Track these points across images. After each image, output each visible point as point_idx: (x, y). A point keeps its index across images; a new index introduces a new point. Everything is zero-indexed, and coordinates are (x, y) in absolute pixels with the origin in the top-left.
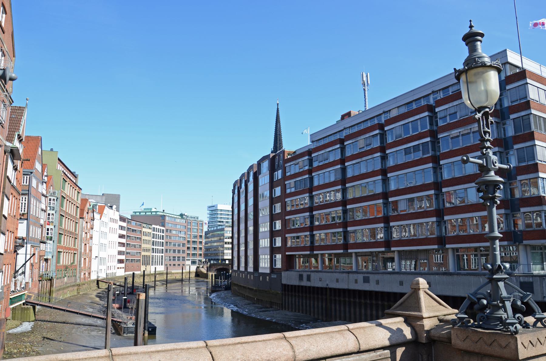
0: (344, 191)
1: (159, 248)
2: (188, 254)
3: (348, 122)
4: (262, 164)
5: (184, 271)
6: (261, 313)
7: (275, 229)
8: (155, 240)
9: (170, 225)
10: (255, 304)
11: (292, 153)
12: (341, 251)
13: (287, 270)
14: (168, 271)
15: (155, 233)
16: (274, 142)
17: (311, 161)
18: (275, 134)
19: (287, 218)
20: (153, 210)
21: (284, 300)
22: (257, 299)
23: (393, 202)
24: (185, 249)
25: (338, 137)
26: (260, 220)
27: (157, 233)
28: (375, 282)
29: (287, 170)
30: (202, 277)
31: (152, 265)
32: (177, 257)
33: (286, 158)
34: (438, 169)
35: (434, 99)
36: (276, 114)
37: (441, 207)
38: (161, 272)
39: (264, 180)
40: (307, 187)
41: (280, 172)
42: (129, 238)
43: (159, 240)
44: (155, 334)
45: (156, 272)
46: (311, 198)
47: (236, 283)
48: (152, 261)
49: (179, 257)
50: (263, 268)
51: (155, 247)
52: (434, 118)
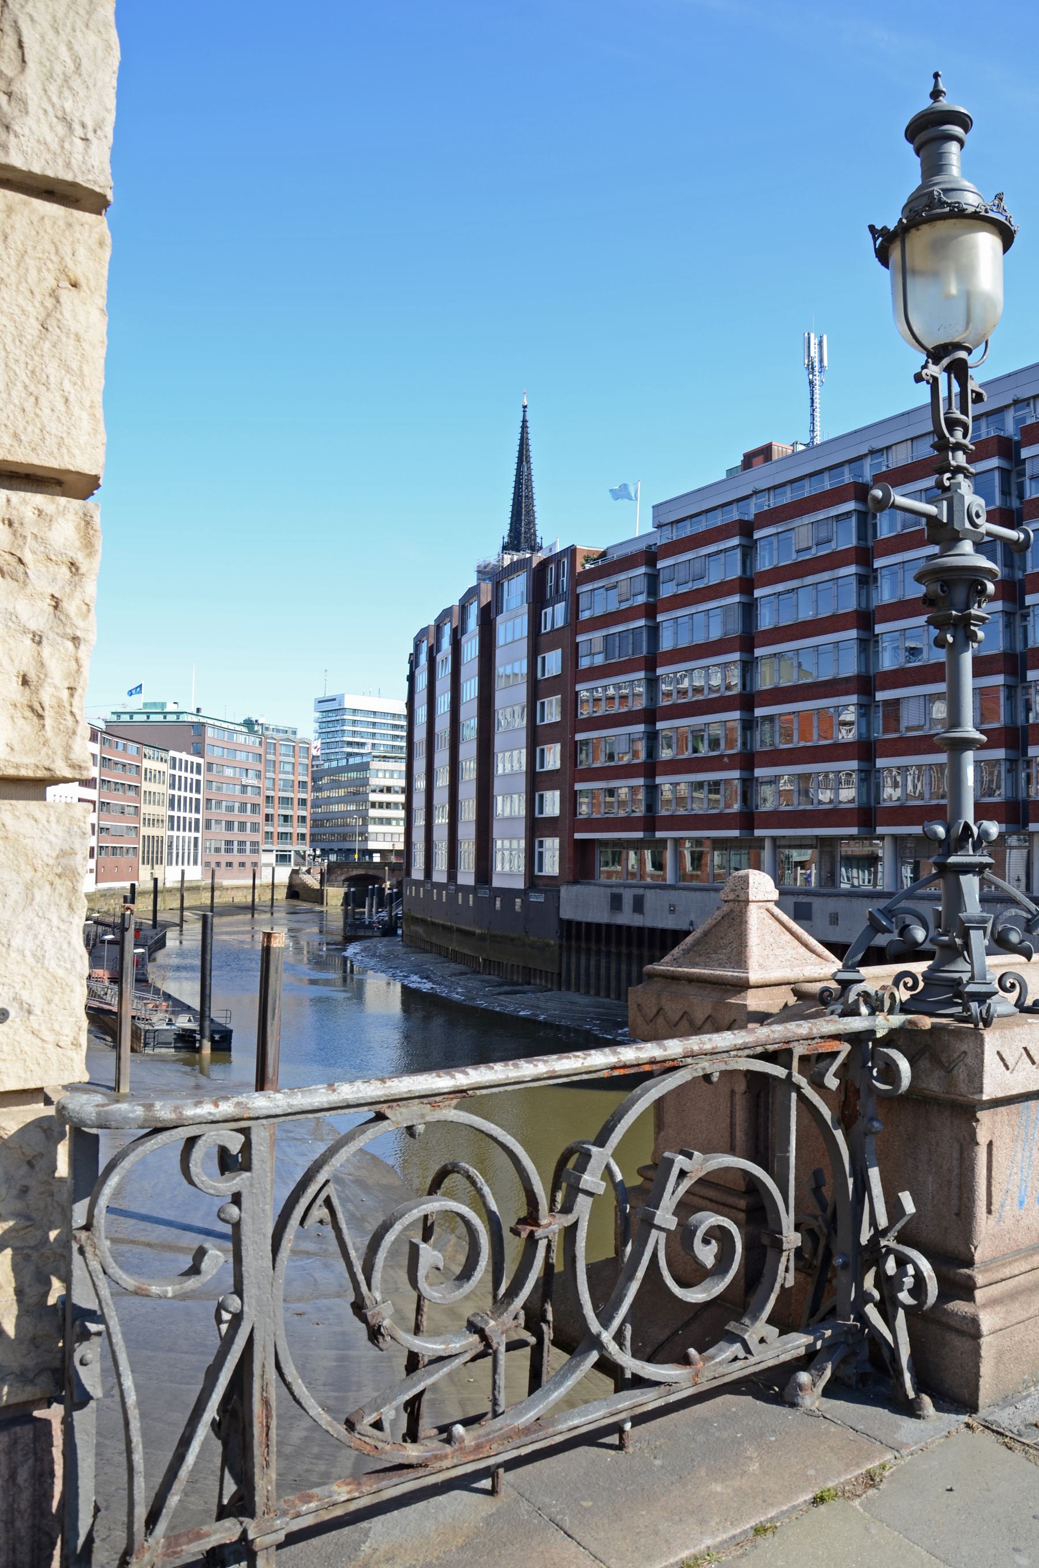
0: (748, 667)
1: (188, 815)
2: (268, 835)
3: (762, 476)
4: (506, 585)
5: (257, 882)
6: (502, 998)
7: (542, 766)
8: (176, 793)
9: (218, 752)
10: (479, 972)
11: (595, 556)
12: (735, 833)
13: (575, 882)
14: (216, 880)
15: (177, 773)
16: (512, 518)
17: (653, 582)
18: (514, 493)
19: (580, 737)
20: (170, 707)
21: (564, 965)
22: (484, 960)
23: (886, 703)
24: (260, 819)
25: (734, 515)
26: (499, 741)
27: (183, 774)
28: (828, 920)
29: (583, 602)
30: (305, 900)
31: (170, 863)
32: (235, 843)
33: (579, 569)
34: (1018, 618)
35: (1017, 421)
36: (519, 436)
37: (1020, 720)
38: (194, 884)
41: (560, 607)
42: (105, 787)
43: (188, 795)
44: (229, 1049)
45: (185, 885)
46: (652, 683)
47: (420, 916)
48: (170, 854)
49: (242, 843)
50: (503, 874)
51: (175, 813)
52: (1013, 476)
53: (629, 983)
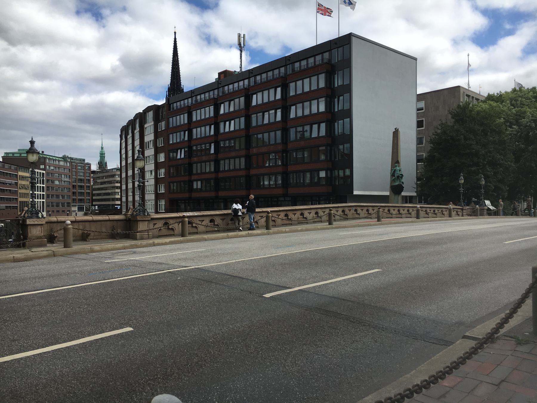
4: (147, 113)
39: (149, 125)
53: (120, 170)
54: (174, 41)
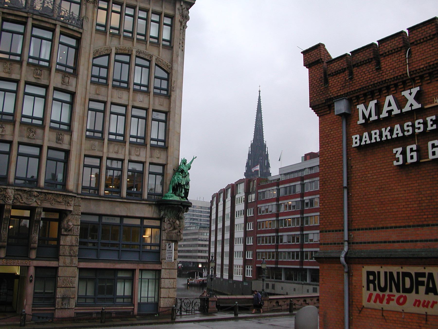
13: (257, 279)
25: (300, 174)
39: (241, 194)
40: (275, 227)
54: (258, 101)
